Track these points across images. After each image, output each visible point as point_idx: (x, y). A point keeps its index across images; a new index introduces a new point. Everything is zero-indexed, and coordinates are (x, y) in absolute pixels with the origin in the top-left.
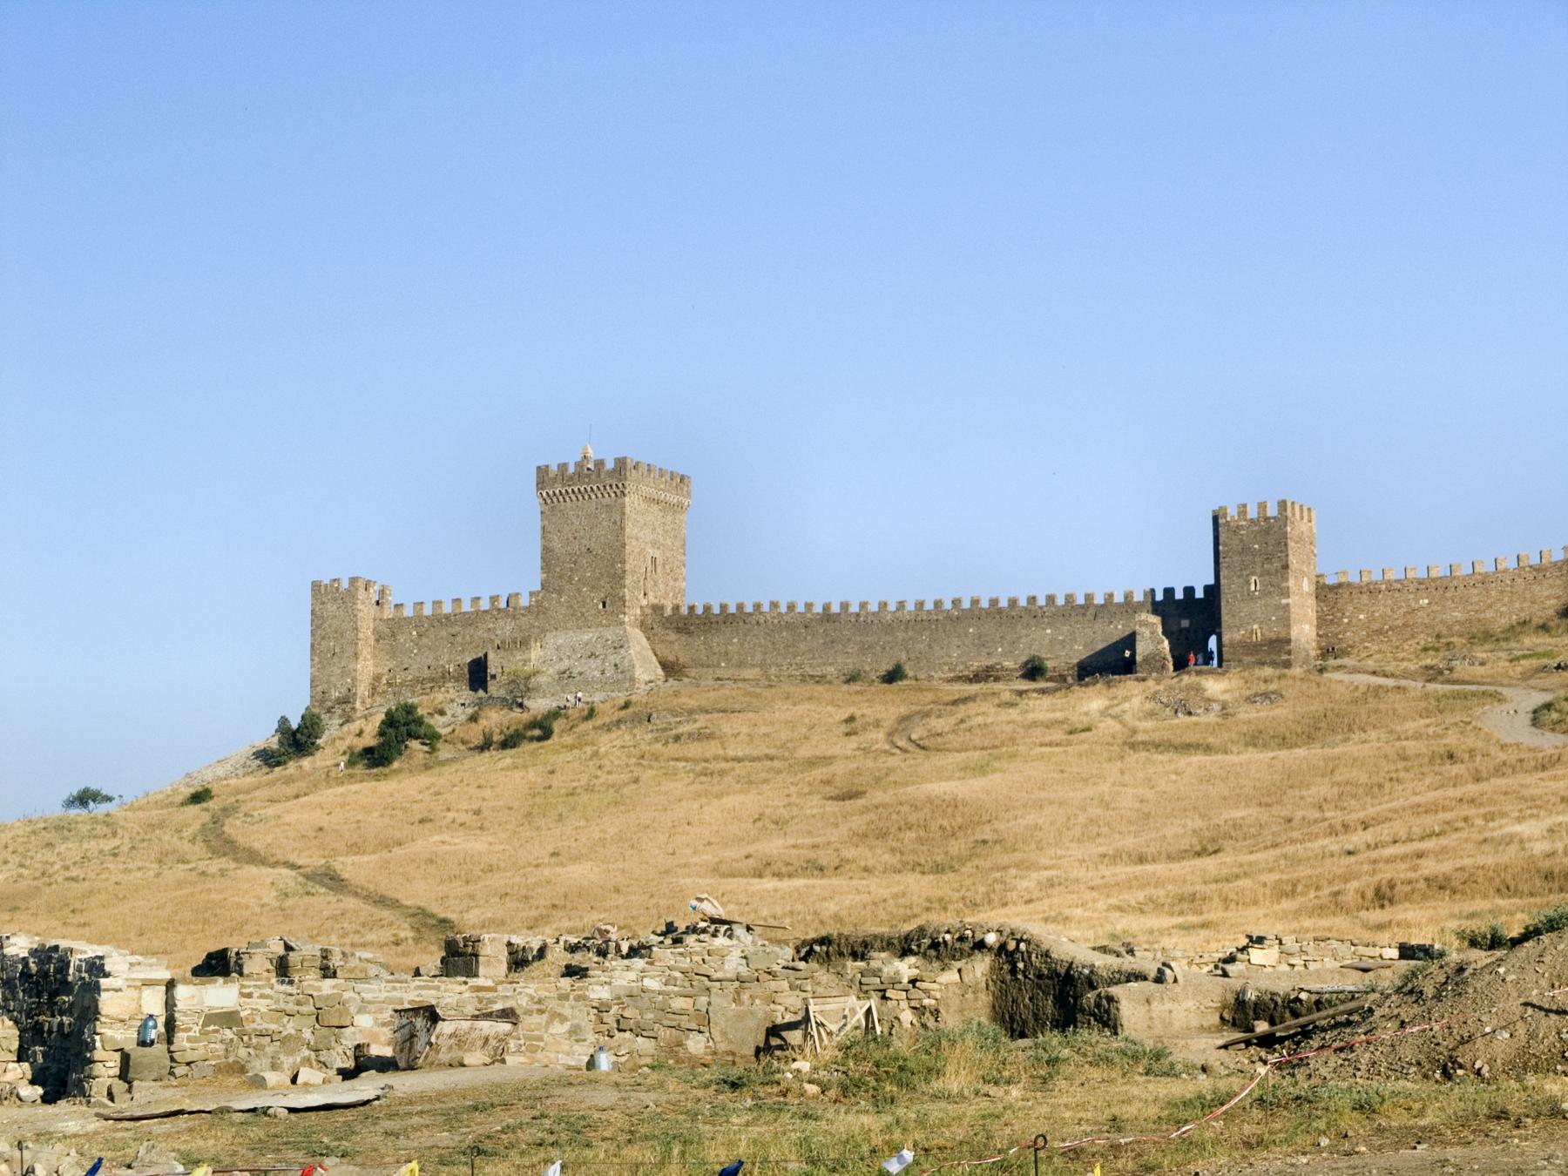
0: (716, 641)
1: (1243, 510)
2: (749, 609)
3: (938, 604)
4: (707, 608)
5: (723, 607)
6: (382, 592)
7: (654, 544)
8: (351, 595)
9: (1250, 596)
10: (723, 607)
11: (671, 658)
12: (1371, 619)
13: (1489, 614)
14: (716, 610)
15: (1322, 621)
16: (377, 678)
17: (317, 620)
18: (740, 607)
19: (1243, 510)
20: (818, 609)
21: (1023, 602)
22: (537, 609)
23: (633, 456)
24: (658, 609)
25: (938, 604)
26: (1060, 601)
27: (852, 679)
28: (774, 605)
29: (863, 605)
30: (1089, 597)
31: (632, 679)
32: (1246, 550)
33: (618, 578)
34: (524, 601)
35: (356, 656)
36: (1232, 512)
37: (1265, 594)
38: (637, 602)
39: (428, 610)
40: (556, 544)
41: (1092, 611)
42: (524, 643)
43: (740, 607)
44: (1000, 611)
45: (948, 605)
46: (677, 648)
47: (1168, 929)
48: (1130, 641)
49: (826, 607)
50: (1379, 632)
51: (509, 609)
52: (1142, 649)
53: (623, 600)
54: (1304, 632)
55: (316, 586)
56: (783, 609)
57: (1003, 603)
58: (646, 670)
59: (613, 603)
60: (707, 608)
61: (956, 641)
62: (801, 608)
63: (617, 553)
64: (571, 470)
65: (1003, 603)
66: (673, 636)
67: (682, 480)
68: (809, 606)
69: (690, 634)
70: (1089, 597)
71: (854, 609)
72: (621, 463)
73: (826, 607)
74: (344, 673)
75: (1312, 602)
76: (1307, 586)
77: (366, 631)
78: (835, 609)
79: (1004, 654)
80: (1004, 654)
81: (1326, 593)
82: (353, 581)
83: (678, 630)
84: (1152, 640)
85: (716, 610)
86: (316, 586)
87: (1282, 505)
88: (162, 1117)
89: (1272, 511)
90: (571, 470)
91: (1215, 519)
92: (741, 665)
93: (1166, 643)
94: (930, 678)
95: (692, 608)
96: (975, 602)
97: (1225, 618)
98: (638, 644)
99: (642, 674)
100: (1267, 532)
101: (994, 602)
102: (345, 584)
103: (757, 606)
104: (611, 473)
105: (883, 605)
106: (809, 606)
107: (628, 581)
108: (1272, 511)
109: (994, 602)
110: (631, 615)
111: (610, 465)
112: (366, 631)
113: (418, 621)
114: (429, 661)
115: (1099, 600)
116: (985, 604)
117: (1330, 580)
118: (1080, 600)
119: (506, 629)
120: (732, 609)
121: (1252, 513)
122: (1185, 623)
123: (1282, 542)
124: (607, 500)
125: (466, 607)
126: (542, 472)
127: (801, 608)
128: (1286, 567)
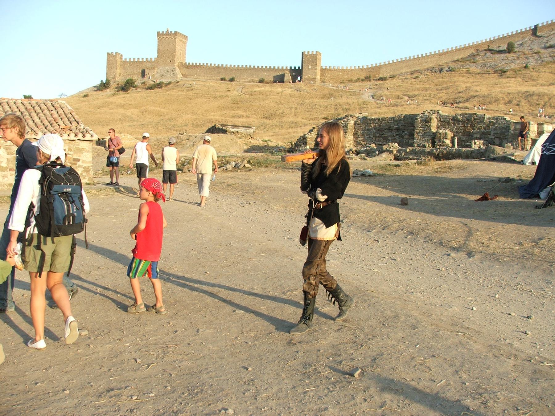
0: (194, 70)
1: (308, 52)
2: (202, 64)
3: (242, 66)
4: (193, 64)
5: (196, 64)
6: (121, 56)
7: (181, 50)
8: (116, 56)
9: (309, 70)
10: (196, 64)
11: (184, 73)
12: (331, 76)
13: (352, 77)
14: (194, 64)
15: (321, 76)
16: (120, 74)
17: (108, 61)
18: (200, 64)
19: (308, 52)
20: (217, 65)
21: (260, 67)
22: (156, 61)
23: (178, 31)
24: (181, 63)
25: (242, 66)
26: (268, 67)
27: (222, 79)
28: (207, 64)
29: (226, 65)
30: (274, 67)
31: (177, 77)
32: (308, 60)
33: (174, 56)
34: (153, 60)
35: (116, 69)
36: (306, 53)
37: (312, 69)
38: (178, 61)
39: (132, 60)
40: (161, 48)
41: (274, 70)
42: (154, 68)
43: (200, 64)
44: (255, 68)
45: (244, 67)
46: (185, 71)
47: (147, 125)
48: (283, 76)
49: (218, 65)
50: (332, 79)
51: (150, 62)
52: (285, 79)
53: (175, 61)
54: (318, 77)
55: (108, 53)
56: (209, 65)
57: (256, 67)
58: (180, 76)
59: (172, 61)
60: (193, 64)
61: (246, 74)
62: (213, 65)
63: (174, 51)
64: (165, 33)
65: (256, 67)
66: (185, 69)
67: (128, 83)
68: (215, 65)
69: (188, 69)
70: (274, 67)
71: (224, 66)
72: (176, 32)
73: (218, 65)
74: (114, 72)
75: (320, 71)
76: (319, 69)
77: (118, 64)
78: (220, 66)
79: (256, 77)
80: (256, 77)
81: (322, 70)
82: (116, 53)
83: (186, 68)
84: (288, 77)
85: (194, 64)
86: (108, 53)
87: (317, 52)
88: (31, 298)
89: (315, 53)
90: (165, 33)
91: (303, 53)
92: (199, 76)
93: (291, 78)
94: (240, 81)
95: (189, 63)
96: (250, 66)
97: (303, 73)
98: (178, 70)
99: (179, 76)
100: (313, 57)
101: (254, 66)
102: (114, 54)
103: (203, 64)
104: (173, 34)
105: (231, 65)
106: (215, 65)
107: (176, 57)
108: (315, 53)
109: (254, 66)
110: (176, 64)
111: (173, 32)
112: (118, 64)
113: (130, 62)
114: (132, 71)
115: (276, 68)
116: (252, 67)
117: (324, 68)
118: (272, 68)
119: (149, 65)
120: (198, 64)
121: (310, 53)
122: (294, 74)
123: (316, 59)
124: (172, 40)
125: (141, 60)
126: (158, 33)
127: (213, 65)
128: (316, 64)
